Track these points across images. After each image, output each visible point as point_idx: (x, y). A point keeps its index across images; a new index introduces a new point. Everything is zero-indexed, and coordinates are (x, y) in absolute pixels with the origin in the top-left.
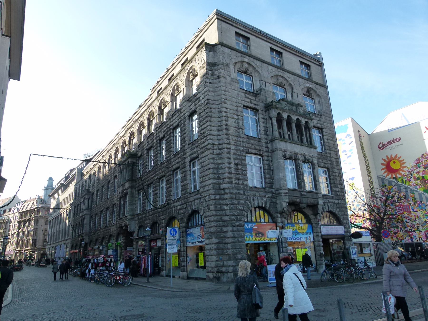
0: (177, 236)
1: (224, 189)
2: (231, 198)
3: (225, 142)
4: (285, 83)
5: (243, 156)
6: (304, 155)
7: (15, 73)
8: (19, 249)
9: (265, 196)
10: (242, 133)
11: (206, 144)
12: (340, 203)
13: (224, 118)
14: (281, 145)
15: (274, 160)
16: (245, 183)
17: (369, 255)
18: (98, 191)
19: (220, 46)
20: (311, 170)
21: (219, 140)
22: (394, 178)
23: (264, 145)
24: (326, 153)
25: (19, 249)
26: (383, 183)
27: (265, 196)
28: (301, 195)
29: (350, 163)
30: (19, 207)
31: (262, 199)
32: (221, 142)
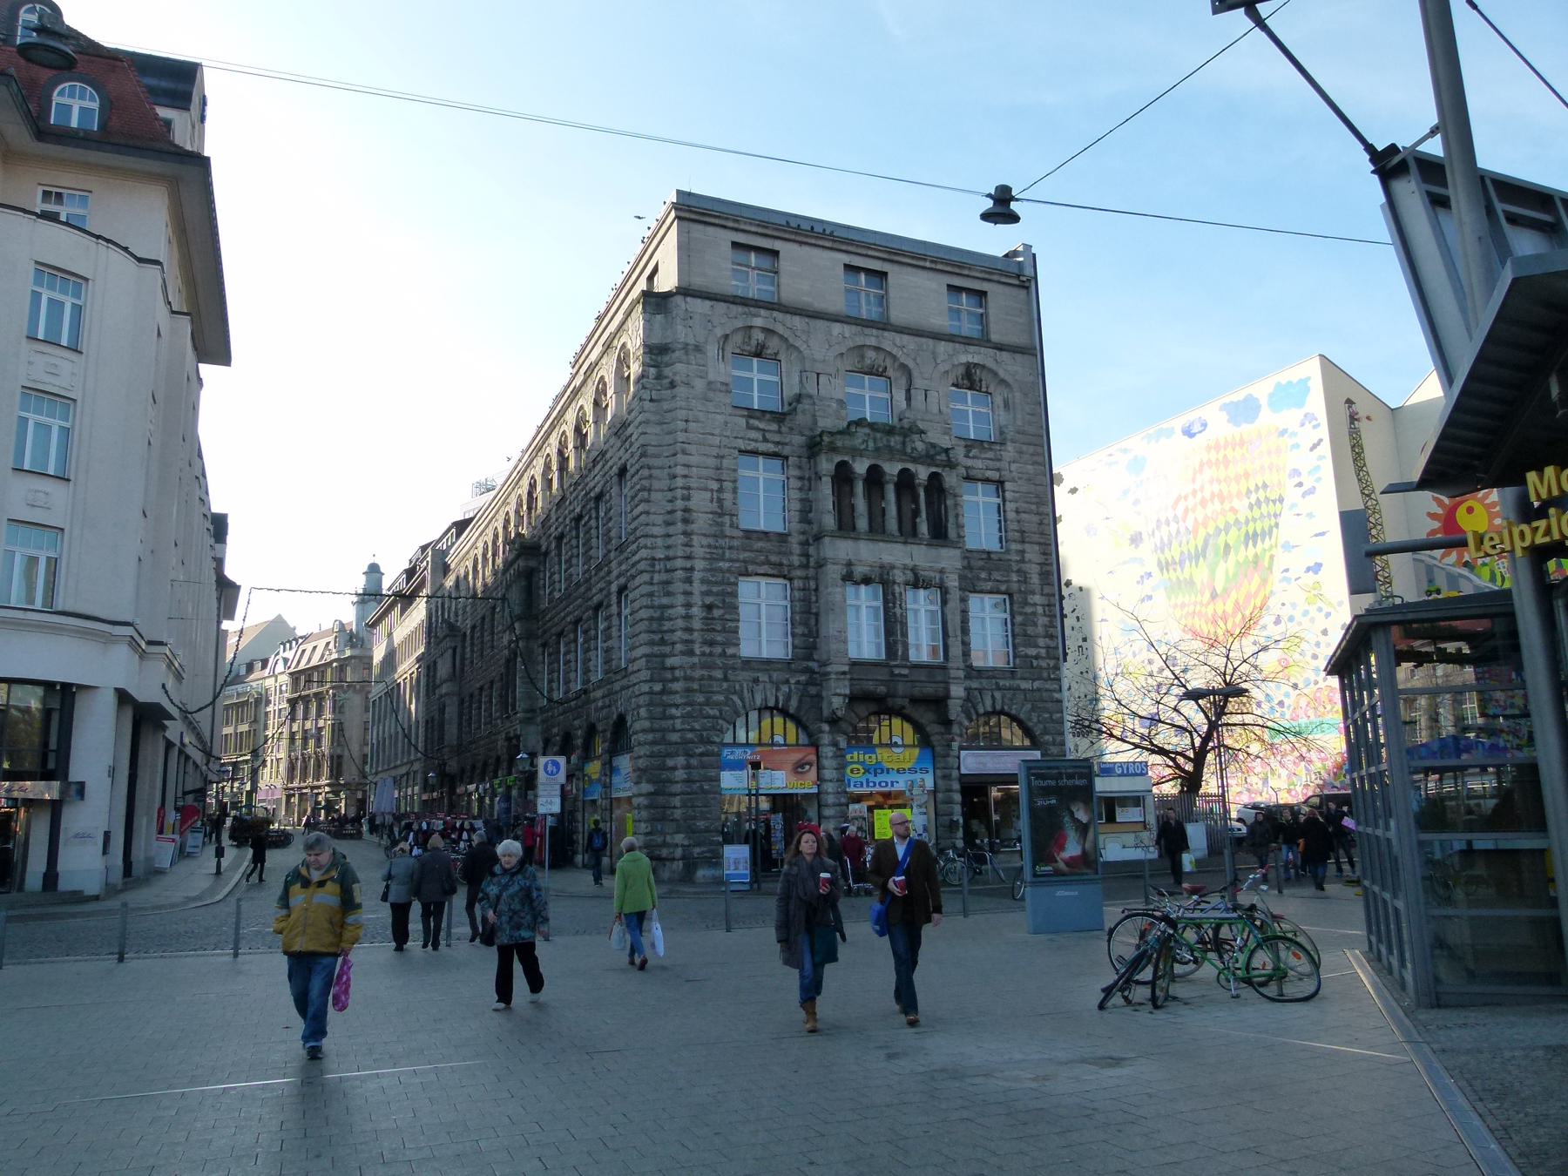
0: (561, 777)
1: (673, 668)
2: (689, 690)
3: (680, 553)
4: (889, 362)
5: (729, 584)
6: (914, 570)
7: (212, 342)
8: (295, 784)
9: (787, 682)
10: (732, 526)
11: (637, 558)
12: (1039, 690)
13: (679, 493)
14: (839, 550)
15: (821, 588)
16: (730, 651)
17: (1140, 827)
18: (473, 628)
19: (679, 299)
20: (937, 608)
21: (668, 547)
22: (1466, 564)
23: (796, 549)
24: (1008, 551)
25: (295, 784)
26: (1431, 581)
27: (787, 682)
28: (892, 674)
29: (1310, 515)
30: (289, 654)
31: (778, 689)
32: (671, 553)
